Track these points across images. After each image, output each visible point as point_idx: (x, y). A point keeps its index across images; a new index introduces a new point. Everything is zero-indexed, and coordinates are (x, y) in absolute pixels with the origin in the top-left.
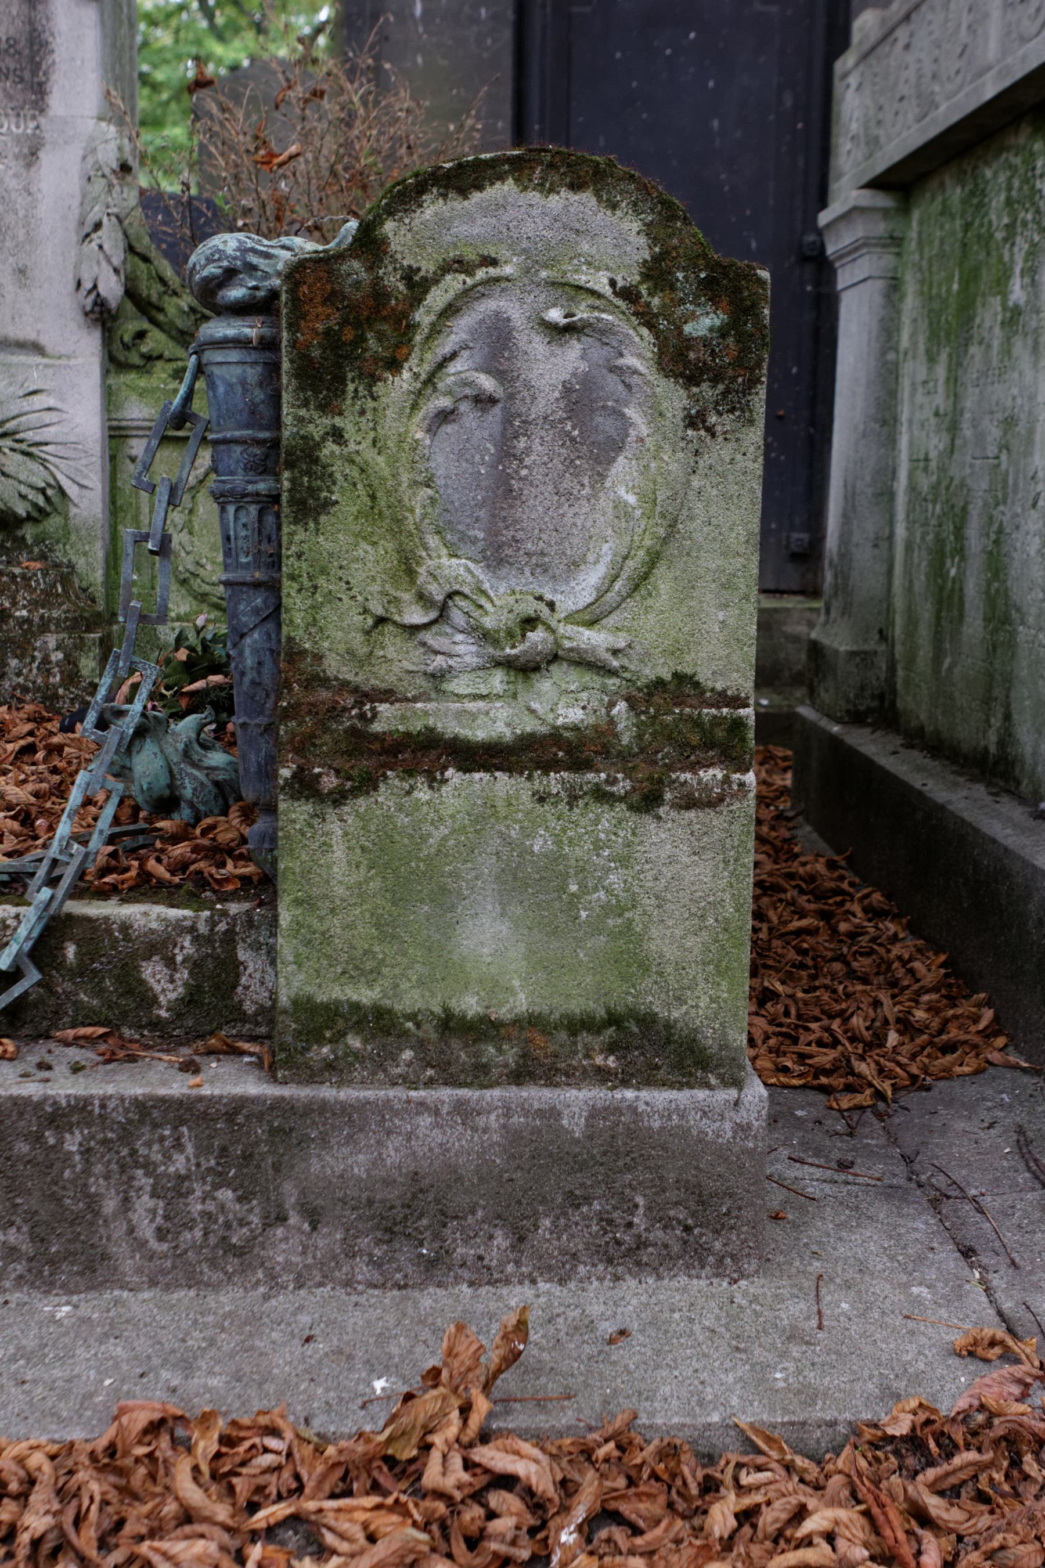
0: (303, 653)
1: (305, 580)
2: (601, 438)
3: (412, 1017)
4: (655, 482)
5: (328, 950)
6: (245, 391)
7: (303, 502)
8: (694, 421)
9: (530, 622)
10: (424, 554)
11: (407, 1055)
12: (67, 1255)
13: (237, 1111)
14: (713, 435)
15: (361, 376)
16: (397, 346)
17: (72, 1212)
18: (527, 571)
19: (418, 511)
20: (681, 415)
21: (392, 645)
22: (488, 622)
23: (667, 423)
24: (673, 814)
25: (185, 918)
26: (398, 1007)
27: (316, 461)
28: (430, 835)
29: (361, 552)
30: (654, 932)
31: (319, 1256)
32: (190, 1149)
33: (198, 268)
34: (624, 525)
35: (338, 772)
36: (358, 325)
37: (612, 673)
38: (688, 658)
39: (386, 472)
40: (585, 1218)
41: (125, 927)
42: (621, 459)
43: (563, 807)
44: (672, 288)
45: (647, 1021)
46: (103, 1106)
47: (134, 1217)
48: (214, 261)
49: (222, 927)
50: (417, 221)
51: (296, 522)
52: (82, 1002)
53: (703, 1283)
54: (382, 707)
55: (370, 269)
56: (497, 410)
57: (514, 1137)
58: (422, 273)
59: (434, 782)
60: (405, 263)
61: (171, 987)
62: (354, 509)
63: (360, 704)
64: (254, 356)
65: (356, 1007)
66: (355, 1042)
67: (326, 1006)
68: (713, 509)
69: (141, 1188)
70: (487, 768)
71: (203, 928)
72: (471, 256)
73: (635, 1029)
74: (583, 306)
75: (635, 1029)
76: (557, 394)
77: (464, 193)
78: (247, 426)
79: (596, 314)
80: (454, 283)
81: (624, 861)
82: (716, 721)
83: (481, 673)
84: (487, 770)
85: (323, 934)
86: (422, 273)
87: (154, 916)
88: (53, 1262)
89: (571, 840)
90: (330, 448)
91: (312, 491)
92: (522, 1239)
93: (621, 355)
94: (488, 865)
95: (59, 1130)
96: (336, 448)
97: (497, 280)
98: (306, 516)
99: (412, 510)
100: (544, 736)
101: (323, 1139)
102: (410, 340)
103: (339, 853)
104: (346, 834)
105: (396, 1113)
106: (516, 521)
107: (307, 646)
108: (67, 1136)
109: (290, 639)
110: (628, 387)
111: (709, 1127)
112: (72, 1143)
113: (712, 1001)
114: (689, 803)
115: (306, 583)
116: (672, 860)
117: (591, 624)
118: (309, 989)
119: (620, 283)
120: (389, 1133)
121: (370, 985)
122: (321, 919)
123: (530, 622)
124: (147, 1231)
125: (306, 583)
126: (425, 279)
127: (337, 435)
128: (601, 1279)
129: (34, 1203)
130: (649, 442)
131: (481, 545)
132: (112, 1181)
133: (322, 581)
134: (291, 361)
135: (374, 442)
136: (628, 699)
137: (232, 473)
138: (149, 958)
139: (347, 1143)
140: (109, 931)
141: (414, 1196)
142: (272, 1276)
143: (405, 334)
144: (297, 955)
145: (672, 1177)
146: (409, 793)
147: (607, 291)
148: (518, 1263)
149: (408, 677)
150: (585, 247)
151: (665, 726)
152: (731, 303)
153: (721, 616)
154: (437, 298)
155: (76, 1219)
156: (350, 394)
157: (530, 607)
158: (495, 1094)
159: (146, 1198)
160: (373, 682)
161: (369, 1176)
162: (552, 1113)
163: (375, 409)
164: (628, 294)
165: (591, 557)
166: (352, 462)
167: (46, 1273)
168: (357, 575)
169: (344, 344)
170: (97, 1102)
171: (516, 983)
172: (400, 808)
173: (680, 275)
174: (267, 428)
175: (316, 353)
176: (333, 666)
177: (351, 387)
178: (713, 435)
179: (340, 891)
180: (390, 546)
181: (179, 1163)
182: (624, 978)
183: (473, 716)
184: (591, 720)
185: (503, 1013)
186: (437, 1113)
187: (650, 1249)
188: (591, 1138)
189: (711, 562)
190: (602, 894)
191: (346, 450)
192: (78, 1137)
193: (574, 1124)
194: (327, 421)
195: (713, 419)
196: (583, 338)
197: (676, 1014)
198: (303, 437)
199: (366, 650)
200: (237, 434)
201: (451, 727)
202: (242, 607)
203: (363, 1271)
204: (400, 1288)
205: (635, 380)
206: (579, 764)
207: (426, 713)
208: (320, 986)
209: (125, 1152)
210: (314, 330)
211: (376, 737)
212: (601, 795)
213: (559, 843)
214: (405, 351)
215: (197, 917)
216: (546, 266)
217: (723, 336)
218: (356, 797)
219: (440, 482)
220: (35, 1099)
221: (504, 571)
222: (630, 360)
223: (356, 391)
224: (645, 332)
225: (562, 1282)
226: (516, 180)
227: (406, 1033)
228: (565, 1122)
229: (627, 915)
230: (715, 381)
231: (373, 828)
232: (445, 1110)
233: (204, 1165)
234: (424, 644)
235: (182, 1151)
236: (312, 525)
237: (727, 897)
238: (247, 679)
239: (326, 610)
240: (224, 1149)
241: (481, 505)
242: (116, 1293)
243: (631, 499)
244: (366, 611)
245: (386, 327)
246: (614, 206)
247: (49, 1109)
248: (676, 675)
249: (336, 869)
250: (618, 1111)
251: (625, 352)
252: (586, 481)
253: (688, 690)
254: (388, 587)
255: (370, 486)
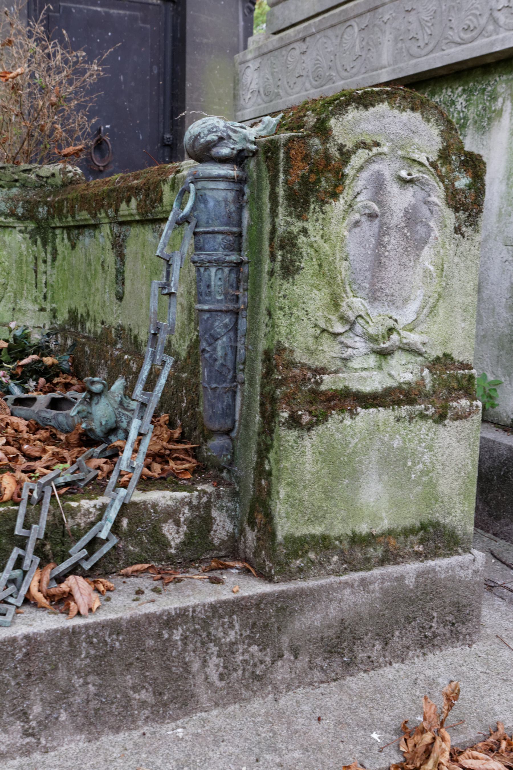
0: (285, 349)
1: (287, 309)
2: (418, 237)
3: (338, 538)
4: (443, 260)
5: (302, 508)
6: (226, 205)
7: (287, 268)
8: (457, 230)
9: (391, 330)
10: (344, 295)
11: (335, 558)
12: (173, 699)
13: (261, 602)
14: (464, 237)
15: (317, 201)
16: (336, 186)
17: (177, 674)
18: (386, 303)
19: (343, 273)
20: (453, 226)
21: (326, 342)
22: (372, 331)
23: (448, 230)
24: (451, 423)
25: (186, 497)
26: (332, 534)
27: (294, 245)
28: (350, 443)
29: (313, 295)
30: (441, 482)
31: (298, 672)
32: (237, 627)
33: (202, 135)
34: (429, 281)
35: (310, 413)
36: (318, 172)
37: (420, 354)
38: (449, 346)
39: (329, 252)
40: (414, 628)
41: (154, 506)
42: (426, 248)
43: (407, 423)
44: (450, 164)
45: (436, 525)
46: (194, 611)
47: (208, 670)
48: (213, 132)
49: (205, 500)
50: (345, 120)
51: (284, 278)
52: (130, 551)
53: (459, 649)
54: (325, 377)
55: (323, 144)
56: (377, 221)
57: (385, 592)
58: (347, 148)
59: (353, 414)
60: (339, 142)
61: (177, 536)
62: (311, 272)
63: (314, 376)
64: (232, 186)
65: (313, 536)
66: (312, 555)
67: (299, 538)
68: (462, 273)
69: (212, 653)
70: (375, 406)
71: (195, 502)
72: (368, 141)
73: (432, 531)
74: (415, 170)
75: (432, 531)
76: (402, 214)
77: (366, 107)
78: (227, 224)
79: (421, 174)
80: (362, 154)
81: (430, 448)
82: (463, 376)
83: (365, 357)
84: (375, 407)
85: (300, 500)
86: (347, 148)
87: (168, 498)
88: (165, 705)
89: (409, 439)
90: (302, 239)
91: (292, 262)
92: (386, 644)
93: (429, 196)
94: (374, 456)
95: (171, 628)
96: (304, 239)
97: (380, 154)
98: (288, 275)
99: (340, 273)
100: (395, 388)
101: (301, 610)
102: (343, 183)
103: (309, 456)
104: (313, 446)
105: (335, 590)
106: (382, 279)
107: (287, 345)
108: (175, 631)
109: (279, 342)
110: (431, 212)
111: (462, 573)
112: (177, 636)
113: (462, 512)
114: (458, 417)
115: (288, 312)
116: (449, 446)
117: (411, 330)
118: (292, 530)
119: (431, 160)
120: (331, 600)
121: (320, 525)
122: (299, 492)
123: (391, 330)
124: (214, 677)
125: (288, 312)
126: (348, 151)
127: (305, 231)
128: (418, 657)
129: (155, 674)
130: (440, 240)
131: (367, 290)
132: (197, 653)
133: (294, 311)
134: (285, 191)
135: (322, 236)
136: (428, 368)
137: (215, 250)
138: (165, 521)
139: (312, 610)
140: (146, 509)
141: (342, 632)
142: (275, 688)
143: (341, 180)
144: (287, 513)
145: (448, 601)
146: (342, 421)
147: (426, 163)
148: (384, 656)
149: (332, 360)
150: (416, 140)
151: (443, 380)
152: (473, 173)
153: (463, 325)
154: (356, 161)
155: (179, 677)
156: (312, 210)
157: (391, 323)
158: (377, 572)
159: (215, 658)
160: (317, 364)
161: (322, 625)
162: (401, 578)
163: (323, 219)
164: (433, 165)
165: (413, 297)
166: (312, 246)
167: (161, 712)
168: (311, 307)
169: (310, 183)
170: (191, 609)
171: (384, 514)
172: (337, 430)
173: (454, 157)
174: (234, 226)
175: (296, 187)
176: (299, 356)
177: (312, 206)
178: (464, 237)
179: (308, 476)
180: (327, 291)
181: (232, 635)
182: (428, 506)
183: (365, 379)
184: (415, 379)
185: (376, 531)
186: (352, 587)
187: (439, 638)
188: (417, 587)
189: (460, 299)
190: (421, 466)
191: (309, 240)
192: (180, 631)
193: (410, 582)
194: (300, 224)
195: (464, 229)
196: (415, 186)
197: (447, 521)
198: (289, 233)
199: (315, 347)
200: (221, 228)
201: (355, 386)
202: (217, 324)
203: (317, 675)
204: (335, 680)
205: (435, 208)
206: (411, 402)
207: (345, 379)
208: (297, 528)
209: (204, 635)
210: (297, 175)
211: (323, 393)
212: (423, 416)
213: (404, 442)
214: (341, 188)
215: (192, 496)
216: (400, 149)
217: (470, 189)
218: (318, 426)
219: (351, 258)
220: (158, 613)
221: (376, 304)
222: (434, 199)
223: (314, 208)
224: (441, 184)
225: (402, 662)
226: (389, 103)
227: (335, 547)
228: (406, 582)
229: (431, 474)
230: (465, 210)
231: (325, 441)
232: (356, 584)
233: (245, 634)
234: (342, 343)
235: (233, 629)
236: (291, 280)
237: (469, 461)
238: (218, 363)
239: (296, 326)
240: (254, 624)
241: (367, 271)
242: (198, 715)
243: (432, 268)
244: (316, 326)
245: (330, 175)
246: (428, 121)
247: (165, 618)
248: (445, 355)
249: (307, 465)
250: (428, 572)
251: (432, 194)
252: (412, 259)
253: (449, 362)
254: (325, 313)
255: (320, 259)
